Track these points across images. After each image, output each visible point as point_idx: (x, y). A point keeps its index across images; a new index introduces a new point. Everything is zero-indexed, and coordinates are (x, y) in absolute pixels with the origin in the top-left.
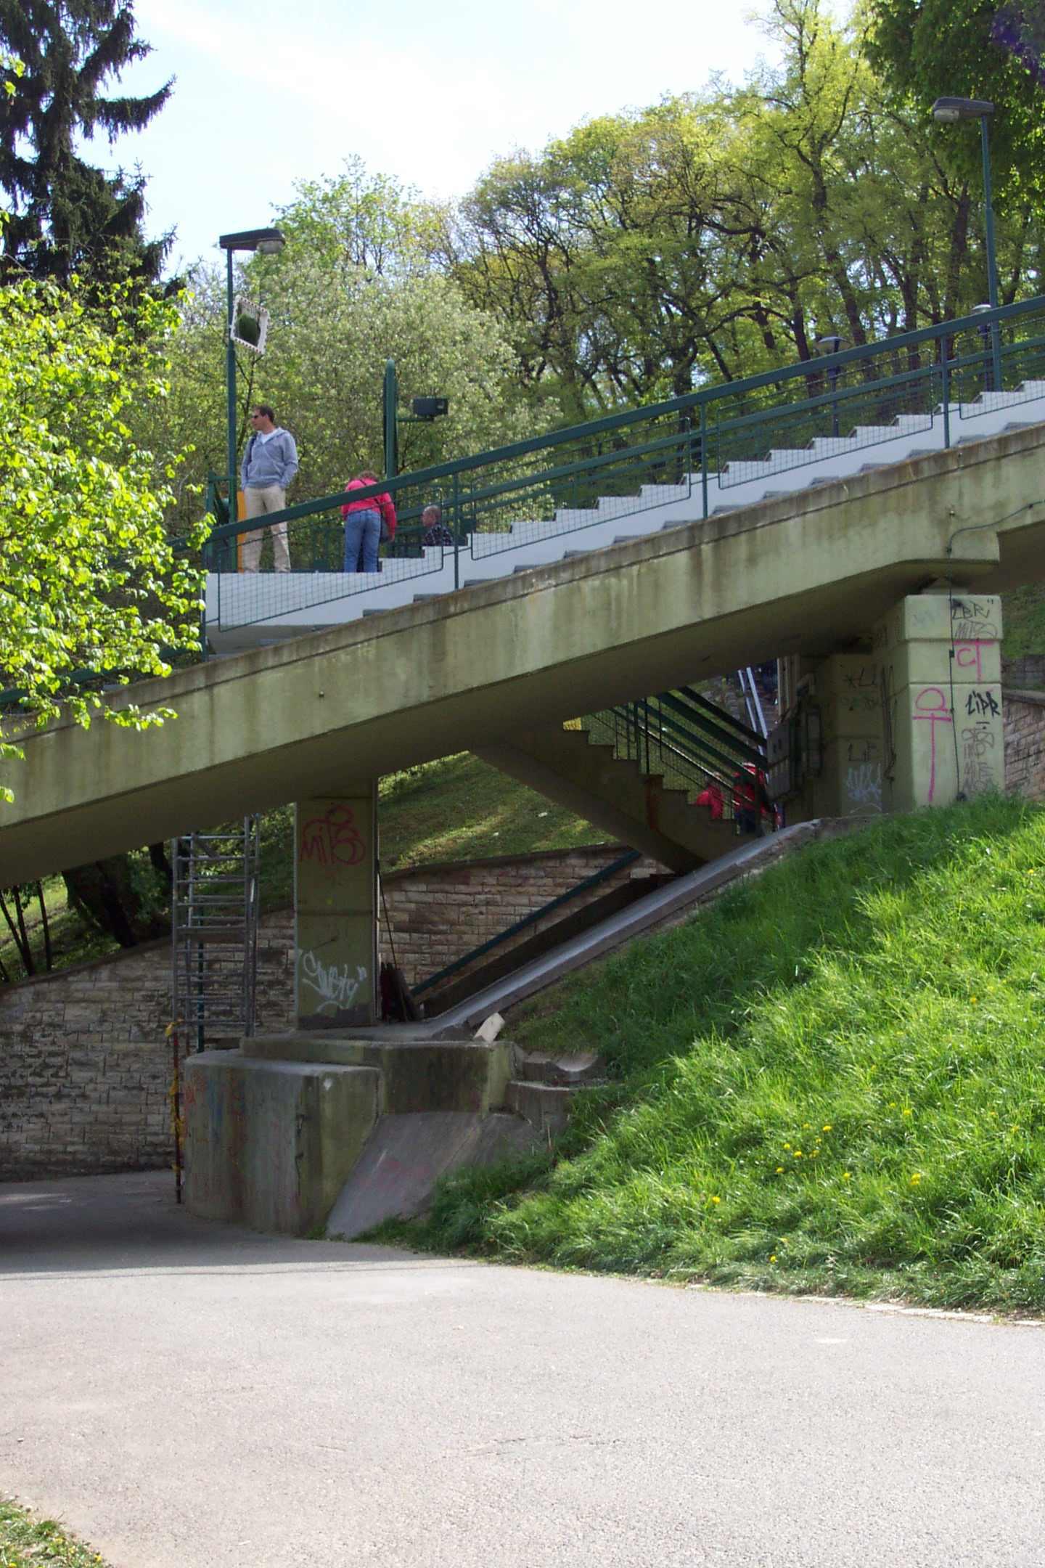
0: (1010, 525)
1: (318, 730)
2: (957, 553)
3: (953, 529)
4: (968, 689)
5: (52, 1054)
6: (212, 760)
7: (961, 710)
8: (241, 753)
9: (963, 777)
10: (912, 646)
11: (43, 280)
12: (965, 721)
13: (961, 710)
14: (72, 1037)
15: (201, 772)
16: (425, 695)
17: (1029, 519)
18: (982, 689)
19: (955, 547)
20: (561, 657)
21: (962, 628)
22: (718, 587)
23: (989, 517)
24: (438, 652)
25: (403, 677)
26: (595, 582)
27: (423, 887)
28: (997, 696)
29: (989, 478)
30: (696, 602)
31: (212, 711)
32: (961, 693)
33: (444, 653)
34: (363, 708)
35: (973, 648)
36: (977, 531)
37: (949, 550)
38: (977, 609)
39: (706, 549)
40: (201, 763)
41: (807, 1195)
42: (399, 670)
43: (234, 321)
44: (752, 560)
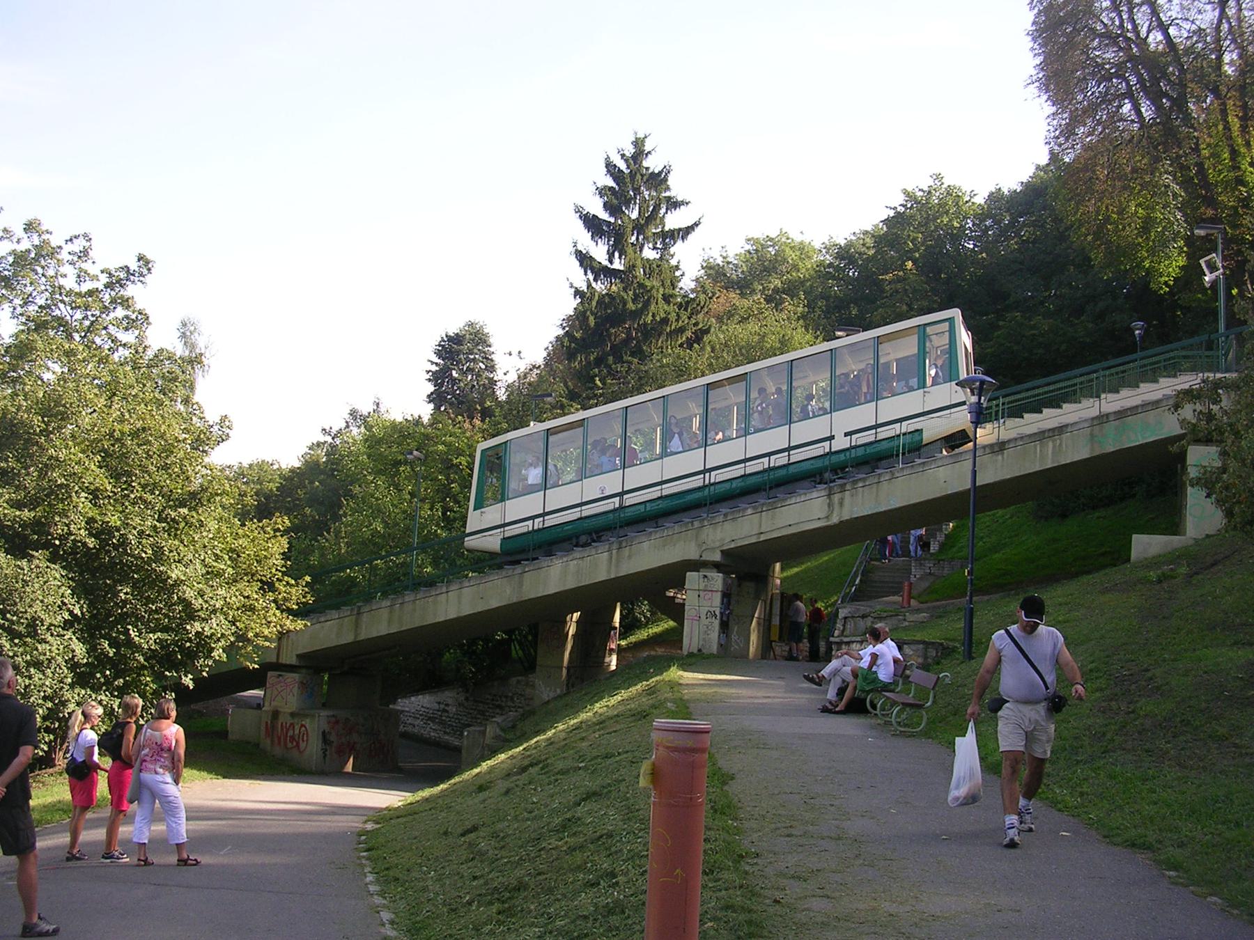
0: (725, 548)
1: (480, 610)
2: (704, 558)
3: (704, 548)
4: (707, 609)
5: (519, 707)
6: (356, 637)
7: (703, 617)
8: (455, 616)
9: (701, 643)
10: (280, 661)
11: (851, 240)
12: (704, 621)
13: (703, 617)
14: (527, 701)
15: (442, 622)
16: (515, 600)
17: (733, 545)
18: (712, 610)
19: (703, 555)
20: (562, 589)
21: (706, 586)
22: (617, 566)
23: (718, 544)
24: (521, 584)
25: (508, 593)
26: (575, 562)
27: (663, 650)
28: (718, 613)
29: (719, 529)
30: (609, 572)
31: (447, 601)
32: (704, 611)
33: (522, 585)
34: (494, 603)
35: (710, 593)
36: (713, 549)
37: (701, 557)
38: (713, 579)
39: (614, 552)
40: (442, 619)
41: (55, 765)
42: (508, 591)
43: (582, 415)
44: (630, 557)
